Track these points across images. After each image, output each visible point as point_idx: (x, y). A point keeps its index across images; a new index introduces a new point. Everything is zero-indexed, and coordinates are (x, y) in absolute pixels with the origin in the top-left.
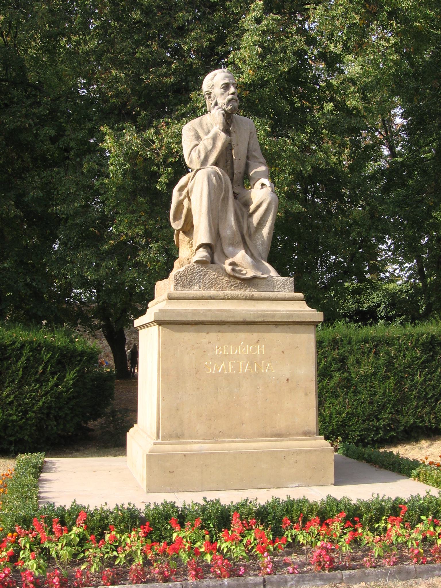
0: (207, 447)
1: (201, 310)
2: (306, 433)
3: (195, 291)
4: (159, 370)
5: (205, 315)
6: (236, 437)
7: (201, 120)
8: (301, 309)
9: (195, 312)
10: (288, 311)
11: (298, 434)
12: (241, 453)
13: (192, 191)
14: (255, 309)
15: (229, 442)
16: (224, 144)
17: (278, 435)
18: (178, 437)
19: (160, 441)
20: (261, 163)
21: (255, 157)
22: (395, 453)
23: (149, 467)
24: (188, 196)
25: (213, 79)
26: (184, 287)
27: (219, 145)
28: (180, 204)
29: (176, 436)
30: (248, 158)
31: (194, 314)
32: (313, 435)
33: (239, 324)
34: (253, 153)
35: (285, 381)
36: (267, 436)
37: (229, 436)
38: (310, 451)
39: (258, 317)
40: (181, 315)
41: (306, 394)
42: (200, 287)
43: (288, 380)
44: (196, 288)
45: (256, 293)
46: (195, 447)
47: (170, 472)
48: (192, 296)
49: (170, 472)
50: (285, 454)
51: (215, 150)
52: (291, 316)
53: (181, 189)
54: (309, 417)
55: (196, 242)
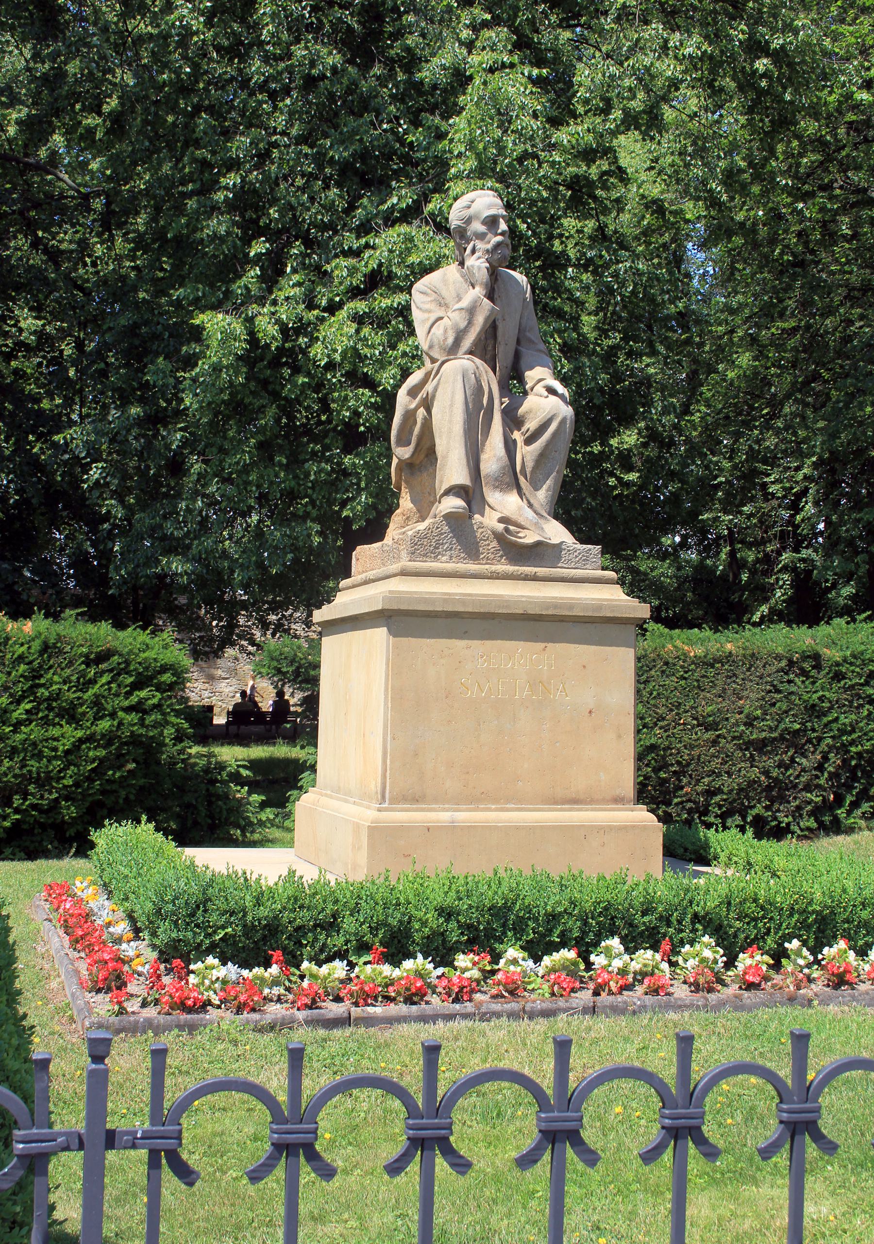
0: (463, 816)
1: (456, 594)
2: (618, 800)
3: (442, 564)
4: (386, 690)
5: (463, 602)
6: (508, 801)
7: (445, 274)
8: (613, 597)
9: (448, 598)
10: (593, 599)
11: (604, 801)
12: (517, 828)
13: (434, 396)
14: (541, 594)
15: (496, 810)
16: (487, 319)
17: (575, 801)
18: (415, 800)
19: (386, 805)
20: (540, 351)
21: (531, 341)
22: (199, 862)
23: (372, 846)
24: (427, 404)
25: (469, 207)
26: (425, 555)
27: (480, 320)
28: (410, 415)
29: (413, 798)
30: (518, 342)
31: (445, 601)
32: (629, 802)
33: (516, 620)
34: (528, 334)
35: (587, 714)
36: (556, 803)
37: (496, 801)
38: (625, 827)
39: (547, 609)
40: (425, 601)
41: (619, 736)
42: (451, 557)
43: (590, 712)
44: (444, 558)
45: (541, 571)
46: (443, 816)
47: (405, 856)
48: (414, 570)
49: (405, 856)
50: (587, 831)
51: (472, 330)
52: (599, 607)
53: (413, 393)
54: (625, 776)
55: (441, 482)
